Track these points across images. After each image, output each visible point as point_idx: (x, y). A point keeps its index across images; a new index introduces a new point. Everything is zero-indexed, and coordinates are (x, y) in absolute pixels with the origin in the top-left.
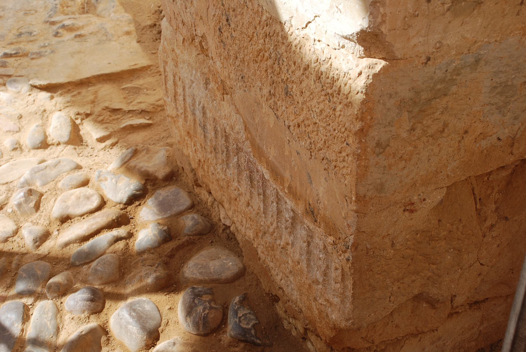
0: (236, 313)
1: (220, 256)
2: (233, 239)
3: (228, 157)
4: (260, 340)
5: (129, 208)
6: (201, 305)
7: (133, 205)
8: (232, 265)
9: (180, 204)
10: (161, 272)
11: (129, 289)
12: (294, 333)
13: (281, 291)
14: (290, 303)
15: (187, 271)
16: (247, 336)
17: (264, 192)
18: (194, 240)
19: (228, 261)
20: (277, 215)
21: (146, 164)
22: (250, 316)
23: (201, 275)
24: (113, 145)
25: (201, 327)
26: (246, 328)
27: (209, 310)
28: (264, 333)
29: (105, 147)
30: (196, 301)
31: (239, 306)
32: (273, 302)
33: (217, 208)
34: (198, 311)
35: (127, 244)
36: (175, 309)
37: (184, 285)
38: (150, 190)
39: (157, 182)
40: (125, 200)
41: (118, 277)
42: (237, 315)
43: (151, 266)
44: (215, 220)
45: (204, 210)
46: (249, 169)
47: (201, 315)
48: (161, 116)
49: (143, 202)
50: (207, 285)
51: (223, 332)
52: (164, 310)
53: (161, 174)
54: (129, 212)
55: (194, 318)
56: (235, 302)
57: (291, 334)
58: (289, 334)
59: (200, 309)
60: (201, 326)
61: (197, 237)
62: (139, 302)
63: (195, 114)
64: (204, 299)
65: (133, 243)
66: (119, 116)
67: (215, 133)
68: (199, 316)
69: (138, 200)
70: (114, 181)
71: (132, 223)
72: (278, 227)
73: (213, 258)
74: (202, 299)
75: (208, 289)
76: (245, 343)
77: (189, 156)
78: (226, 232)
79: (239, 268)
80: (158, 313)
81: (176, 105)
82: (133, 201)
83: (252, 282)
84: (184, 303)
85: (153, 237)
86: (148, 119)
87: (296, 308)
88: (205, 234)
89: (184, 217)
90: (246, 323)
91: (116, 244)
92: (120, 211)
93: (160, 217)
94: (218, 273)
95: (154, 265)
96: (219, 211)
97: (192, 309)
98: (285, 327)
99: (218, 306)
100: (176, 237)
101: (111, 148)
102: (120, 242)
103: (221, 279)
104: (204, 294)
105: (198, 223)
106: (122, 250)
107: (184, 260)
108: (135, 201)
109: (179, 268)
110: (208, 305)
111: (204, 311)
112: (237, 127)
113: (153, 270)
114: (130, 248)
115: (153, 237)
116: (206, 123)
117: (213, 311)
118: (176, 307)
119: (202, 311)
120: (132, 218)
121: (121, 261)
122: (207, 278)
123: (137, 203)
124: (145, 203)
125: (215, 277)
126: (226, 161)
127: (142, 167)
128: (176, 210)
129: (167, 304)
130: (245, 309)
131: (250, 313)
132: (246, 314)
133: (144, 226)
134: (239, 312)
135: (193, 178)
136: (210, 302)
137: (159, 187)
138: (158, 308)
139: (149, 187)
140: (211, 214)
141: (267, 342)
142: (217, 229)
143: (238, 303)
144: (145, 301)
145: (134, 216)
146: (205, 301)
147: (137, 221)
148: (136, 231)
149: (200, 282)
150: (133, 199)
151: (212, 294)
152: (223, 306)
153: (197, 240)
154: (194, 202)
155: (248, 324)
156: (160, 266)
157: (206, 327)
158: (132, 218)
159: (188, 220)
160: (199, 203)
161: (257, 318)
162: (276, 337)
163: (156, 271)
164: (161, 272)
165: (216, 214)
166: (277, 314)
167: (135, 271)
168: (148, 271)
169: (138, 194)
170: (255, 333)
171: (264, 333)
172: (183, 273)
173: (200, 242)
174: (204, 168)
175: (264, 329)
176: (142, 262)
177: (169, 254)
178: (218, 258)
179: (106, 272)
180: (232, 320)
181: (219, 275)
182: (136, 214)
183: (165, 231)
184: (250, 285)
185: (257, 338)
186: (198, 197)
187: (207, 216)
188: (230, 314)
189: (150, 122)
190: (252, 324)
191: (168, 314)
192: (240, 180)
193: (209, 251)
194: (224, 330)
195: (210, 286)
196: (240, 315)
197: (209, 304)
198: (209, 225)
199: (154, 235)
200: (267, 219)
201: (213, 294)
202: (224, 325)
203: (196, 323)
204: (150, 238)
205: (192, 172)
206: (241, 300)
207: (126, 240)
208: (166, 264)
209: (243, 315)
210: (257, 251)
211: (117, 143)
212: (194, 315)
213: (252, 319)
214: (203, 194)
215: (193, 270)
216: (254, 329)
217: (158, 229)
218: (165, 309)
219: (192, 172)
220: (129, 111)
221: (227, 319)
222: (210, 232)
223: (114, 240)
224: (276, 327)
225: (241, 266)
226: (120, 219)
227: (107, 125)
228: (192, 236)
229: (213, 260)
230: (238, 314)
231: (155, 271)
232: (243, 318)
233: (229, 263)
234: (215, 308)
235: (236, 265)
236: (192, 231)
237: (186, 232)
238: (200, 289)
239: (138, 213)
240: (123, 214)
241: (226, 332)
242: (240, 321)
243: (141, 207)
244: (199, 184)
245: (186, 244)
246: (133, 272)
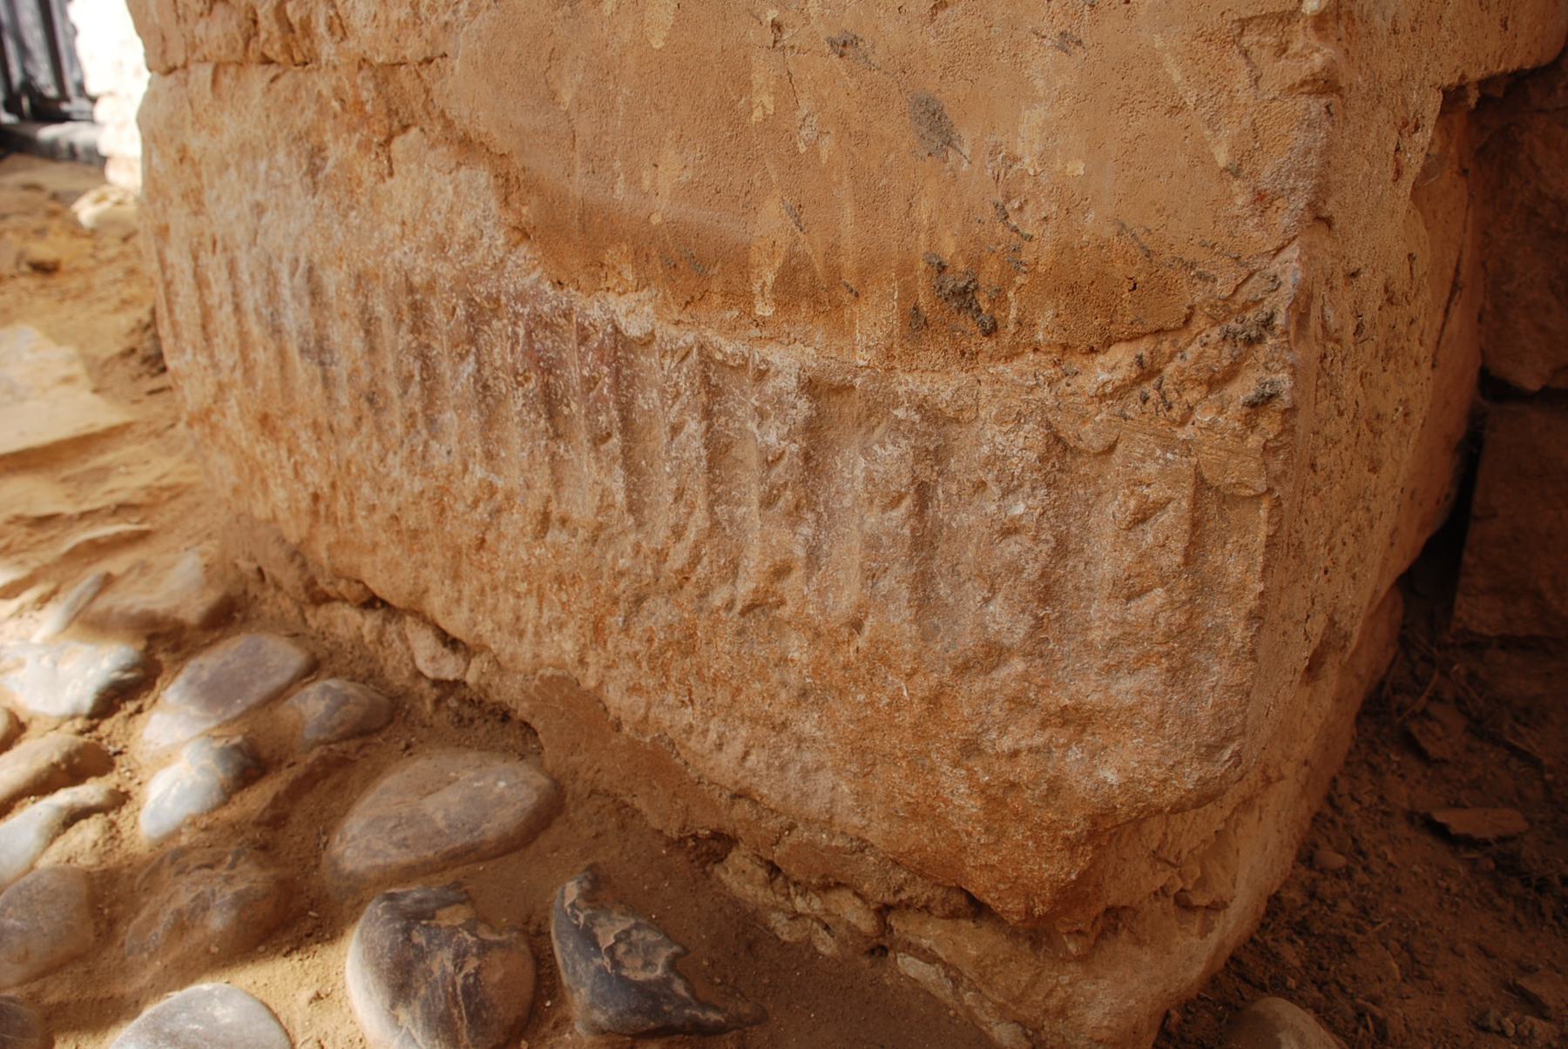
0: (588, 937)
1: (453, 774)
2: (477, 722)
3: (431, 390)
4: (716, 1009)
5: (106, 727)
6: (440, 946)
7: (119, 716)
8: (509, 787)
9: (271, 671)
10: (252, 876)
11: (144, 979)
12: (826, 946)
13: (744, 807)
14: (802, 834)
15: (348, 853)
16: (665, 1008)
17: (626, 410)
18: (345, 752)
19: (490, 779)
20: (710, 469)
21: (144, 598)
22: (642, 935)
23: (404, 850)
24: (44, 600)
25: (464, 1032)
26: (649, 982)
27: (478, 956)
28: (718, 980)
29: (21, 608)
30: (419, 938)
31: (589, 912)
32: (703, 865)
33: (397, 644)
34: (437, 974)
35: (113, 824)
36: (336, 995)
37: (349, 902)
38: (165, 665)
39: (186, 636)
40: (87, 704)
41: (93, 939)
42: (596, 945)
43: (210, 866)
44: (401, 679)
45: (353, 665)
46: (540, 359)
47: (454, 984)
48: (172, 510)
49: (150, 700)
50: (435, 877)
51: (556, 1026)
52: (295, 1008)
53: (193, 611)
54: (109, 736)
55: (426, 1004)
56: (567, 902)
57: (816, 953)
58: (807, 956)
59: (442, 962)
60: (463, 1027)
61: (353, 744)
62: (186, 1005)
63: (280, 331)
64: (448, 922)
65: (131, 819)
66: (53, 532)
67: (368, 332)
68: (445, 991)
69: (133, 698)
70: (46, 662)
71: (122, 766)
72: (716, 524)
73: (430, 787)
74: (438, 926)
75: (448, 888)
76: (666, 1040)
77: (275, 519)
78: (448, 708)
79: (538, 788)
80: (273, 1024)
81: (211, 356)
82: (116, 701)
83: (601, 823)
84: (372, 958)
85: (199, 778)
86: (138, 523)
87: (839, 842)
88: (379, 730)
89: (294, 700)
90: (639, 963)
91: (71, 831)
92: (74, 737)
93: (213, 724)
94: (467, 827)
95: (220, 861)
96: (408, 648)
97: (408, 972)
98: (785, 937)
99: (505, 937)
100: (280, 762)
101: (40, 609)
102: (83, 822)
103: (482, 842)
104: (439, 908)
105: (346, 700)
106: (95, 845)
107: (327, 823)
108: (124, 701)
109: (317, 849)
110: (471, 939)
111: (459, 966)
112: (461, 226)
113: (220, 879)
114: (125, 835)
115: (199, 778)
116: (325, 326)
117: (496, 957)
118: (340, 985)
119: (450, 968)
120: (120, 753)
121: (97, 882)
122: (430, 854)
123: (131, 706)
124: (155, 701)
125: (461, 840)
126: (425, 408)
127: (132, 606)
128: (259, 690)
129: (300, 985)
130: (615, 915)
131: (637, 926)
132: (627, 932)
133: (164, 759)
134: (598, 931)
135: (300, 578)
136: (475, 928)
137: (195, 650)
138: (269, 1008)
139: (161, 657)
140: (382, 669)
141: (746, 1009)
142: (412, 706)
143: (581, 903)
144: (210, 994)
145: (125, 746)
146: (454, 930)
147: (137, 757)
148: (140, 784)
149: (408, 873)
150: (116, 697)
151: (468, 900)
152: (525, 932)
153: (357, 752)
154: (314, 654)
155: (647, 964)
156: (243, 859)
157: (485, 1023)
158: (120, 753)
159: (311, 701)
160: (331, 655)
161: (667, 936)
162: (766, 981)
163: (233, 877)
164: (251, 877)
165: (399, 662)
166: (735, 902)
167: (152, 901)
168: (201, 888)
169: (130, 679)
170: (687, 989)
171: (718, 980)
172: (335, 863)
173: (366, 756)
174: (334, 513)
175: (713, 963)
176: (172, 863)
177: (267, 816)
178: (449, 783)
179: (40, 928)
180: (581, 968)
181: (471, 831)
182: (132, 739)
183: (237, 747)
184: (597, 836)
185: (705, 1005)
186: (325, 639)
187: (372, 676)
188: (563, 950)
189: (145, 527)
190: (661, 961)
191: (316, 1020)
192: (494, 448)
193: (408, 772)
194: (559, 1014)
195: (449, 877)
196: (607, 940)
197: (473, 935)
198: (382, 700)
199: (203, 769)
200: (648, 528)
201: (469, 899)
202: (550, 996)
203: (441, 1019)
204: (188, 783)
205: (292, 561)
206: (588, 891)
207: (107, 814)
208: (264, 850)
209: (618, 939)
210: (600, 701)
211: (55, 592)
212: (422, 992)
213: (656, 945)
214: (339, 621)
215: (369, 840)
216: (680, 976)
217: (212, 749)
218: (296, 1006)
219: (292, 561)
220: (83, 516)
221: (553, 973)
222: (391, 721)
223: (60, 821)
224: (750, 947)
225: (542, 781)
226: (77, 760)
227: (21, 556)
228: (335, 742)
229: (431, 793)
230: (600, 939)
231: (229, 880)
232: (622, 948)
233: (495, 784)
234: (500, 945)
235: (525, 782)
236: (333, 728)
237: (310, 735)
238: (417, 895)
239: (136, 734)
240: (86, 745)
241: (567, 1020)
242: (616, 964)
243: (144, 715)
244: (322, 591)
245: (319, 769)
246: (147, 908)
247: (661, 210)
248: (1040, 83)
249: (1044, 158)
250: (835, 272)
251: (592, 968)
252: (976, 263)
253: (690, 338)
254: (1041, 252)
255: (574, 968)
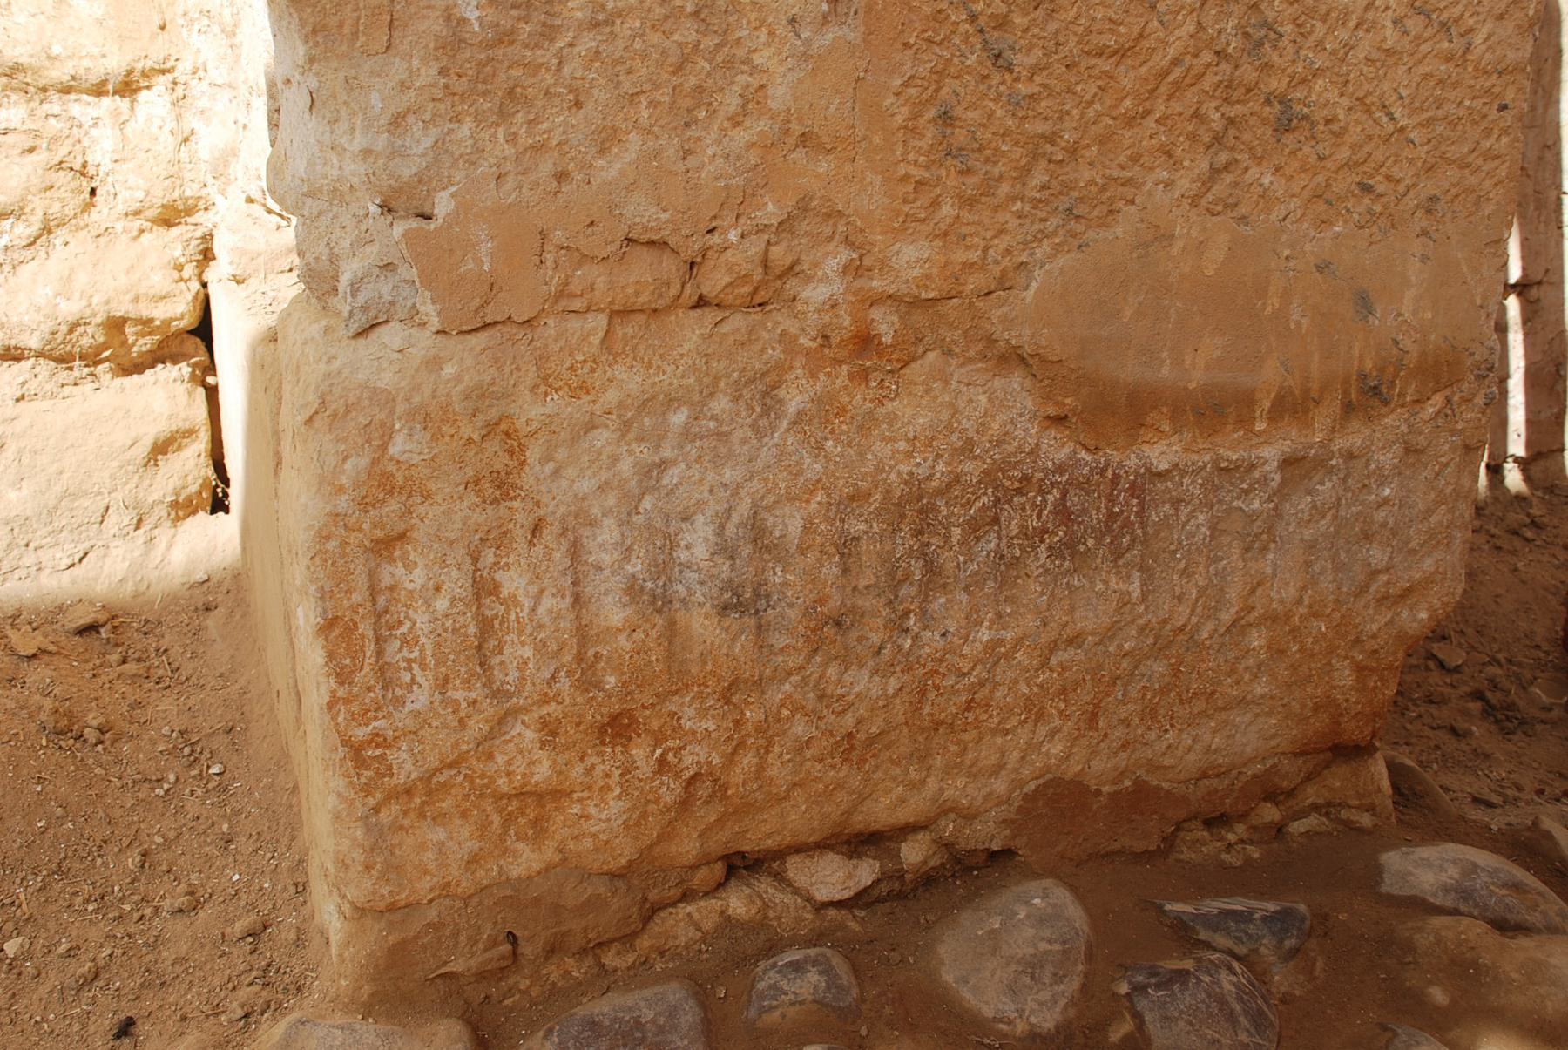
247: (1196, 379)
248: (1413, 278)
249: (1415, 313)
250: (1306, 392)
251: (1258, 922)
252: (1382, 370)
253: (1207, 458)
254: (1411, 360)
255: (1246, 933)
